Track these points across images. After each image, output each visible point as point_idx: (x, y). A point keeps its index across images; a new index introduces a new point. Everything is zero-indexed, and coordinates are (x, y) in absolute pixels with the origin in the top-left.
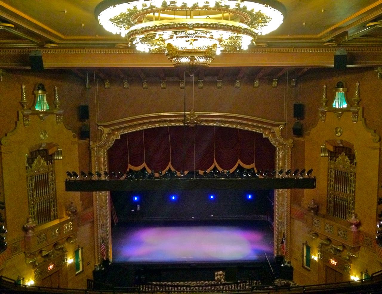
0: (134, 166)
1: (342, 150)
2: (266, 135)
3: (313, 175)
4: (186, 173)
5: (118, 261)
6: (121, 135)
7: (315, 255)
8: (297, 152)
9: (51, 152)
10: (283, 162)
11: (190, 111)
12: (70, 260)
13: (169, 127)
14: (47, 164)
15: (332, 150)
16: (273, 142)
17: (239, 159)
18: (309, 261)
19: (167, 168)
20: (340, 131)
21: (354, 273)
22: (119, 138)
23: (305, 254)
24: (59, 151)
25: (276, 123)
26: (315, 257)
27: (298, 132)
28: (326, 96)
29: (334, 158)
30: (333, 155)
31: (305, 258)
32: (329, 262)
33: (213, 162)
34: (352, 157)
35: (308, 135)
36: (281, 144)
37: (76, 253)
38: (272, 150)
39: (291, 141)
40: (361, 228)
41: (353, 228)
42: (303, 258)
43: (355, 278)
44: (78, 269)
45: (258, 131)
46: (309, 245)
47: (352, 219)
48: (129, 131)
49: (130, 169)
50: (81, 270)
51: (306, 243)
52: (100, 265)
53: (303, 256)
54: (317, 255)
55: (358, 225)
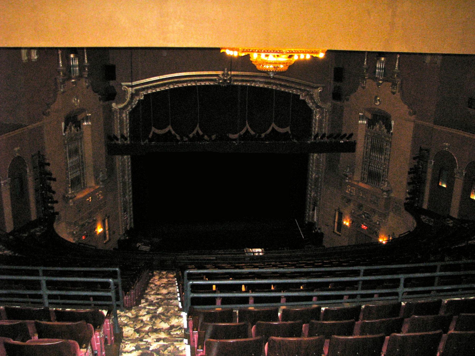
1: (379, 118)
3: (352, 139)
4: (214, 137)
6: (145, 95)
7: (347, 221)
8: (337, 116)
10: (320, 122)
13: (198, 86)
14: (77, 130)
15: (370, 118)
16: (310, 105)
17: (274, 121)
18: (340, 224)
19: (195, 132)
20: (379, 100)
21: (382, 236)
22: (142, 98)
23: (336, 220)
24: (88, 116)
25: (315, 85)
26: (347, 223)
27: (337, 95)
28: (367, 63)
29: (372, 126)
30: (371, 123)
31: (336, 224)
34: (389, 127)
35: (347, 100)
36: (318, 107)
37: (104, 222)
38: (309, 112)
39: (329, 104)
40: (392, 195)
41: (385, 195)
42: (334, 224)
43: (383, 240)
44: (105, 237)
46: (342, 210)
49: (154, 133)
51: (339, 209)
52: (124, 235)
53: (334, 221)
54: (349, 220)
55: (388, 192)
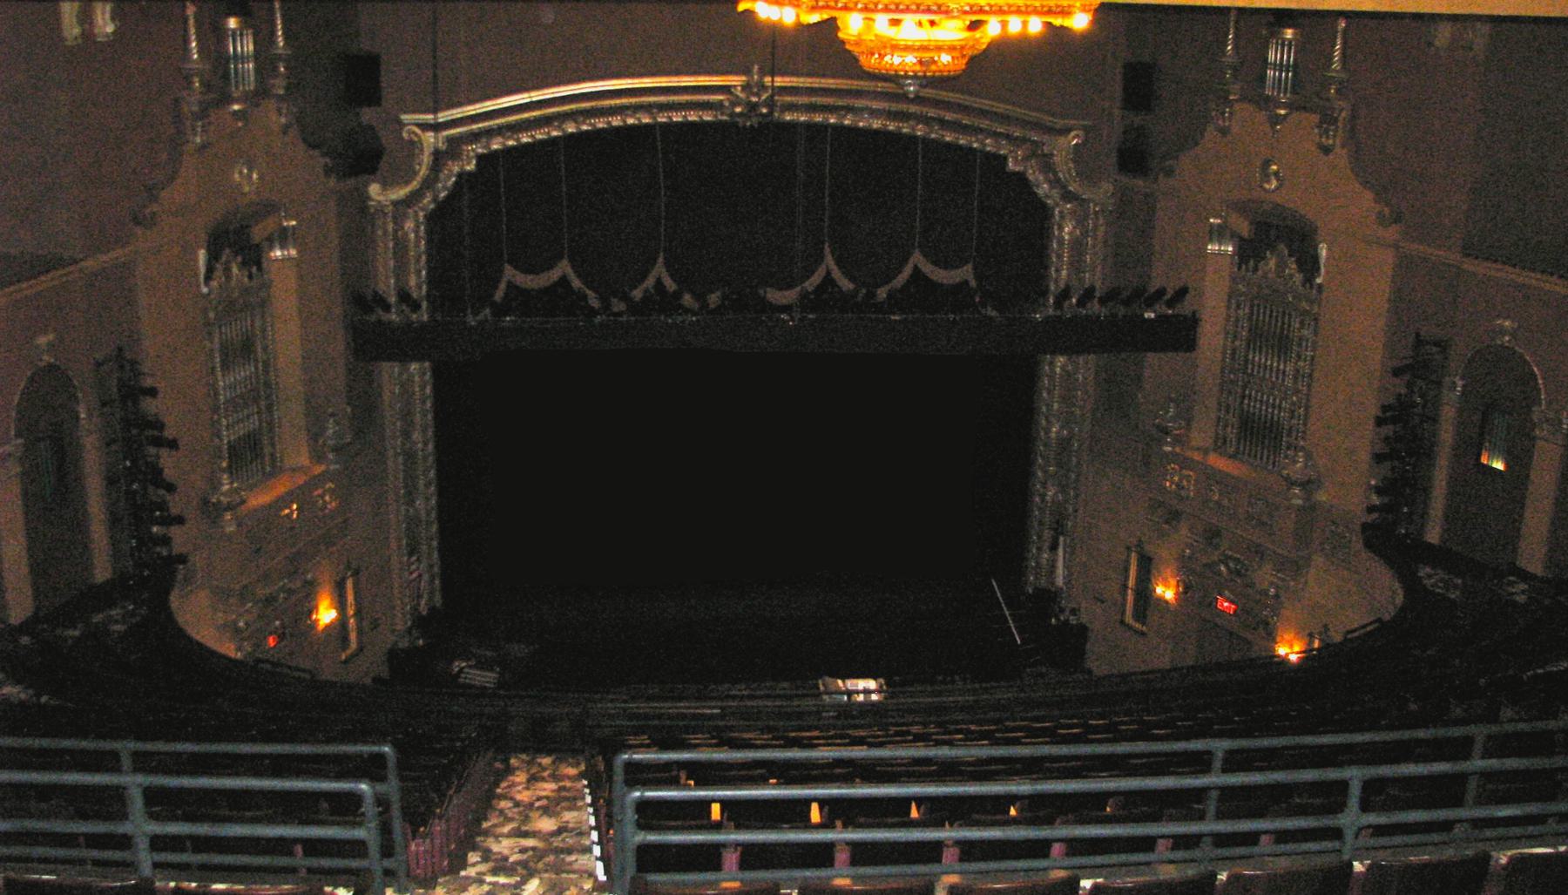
0: (527, 271)
1: (1278, 235)
2: (1016, 161)
3: (1185, 308)
4: (714, 299)
5: (306, 664)
6: (480, 158)
7: (1166, 585)
8: (1133, 226)
9: (257, 233)
10: (1076, 251)
11: (746, 71)
12: (326, 615)
13: (662, 125)
14: (250, 277)
15: (1245, 234)
16: (1043, 189)
18: (1144, 595)
19: (650, 282)
20: (1276, 174)
22: (471, 167)
23: (1131, 583)
24: (285, 229)
25: (1060, 123)
26: (1166, 592)
28: (1236, 47)
29: (1252, 263)
30: (1249, 252)
32: (1212, 604)
33: (820, 258)
34: (1309, 265)
35: (1169, 173)
36: (1068, 196)
38: (1039, 214)
40: (1322, 497)
41: (1297, 497)
43: (1289, 650)
44: (345, 640)
45: (989, 145)
46: (1149, 549)
47: (1297, 467)
48: (511, 143)
49: (510, 285)
50: (354, 645)
51: (1140, 544)
52: (409, 631)
53: (1125, 587)
54: (1173, 582)
55: (1308, 485)
